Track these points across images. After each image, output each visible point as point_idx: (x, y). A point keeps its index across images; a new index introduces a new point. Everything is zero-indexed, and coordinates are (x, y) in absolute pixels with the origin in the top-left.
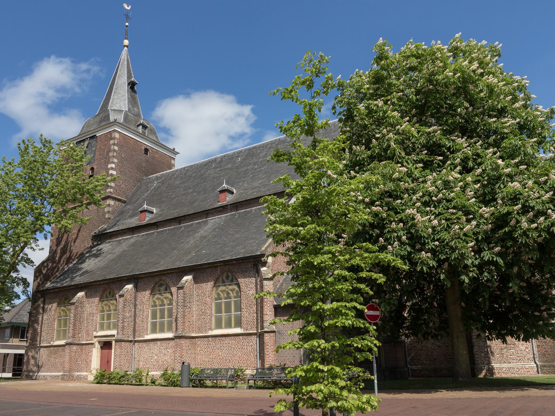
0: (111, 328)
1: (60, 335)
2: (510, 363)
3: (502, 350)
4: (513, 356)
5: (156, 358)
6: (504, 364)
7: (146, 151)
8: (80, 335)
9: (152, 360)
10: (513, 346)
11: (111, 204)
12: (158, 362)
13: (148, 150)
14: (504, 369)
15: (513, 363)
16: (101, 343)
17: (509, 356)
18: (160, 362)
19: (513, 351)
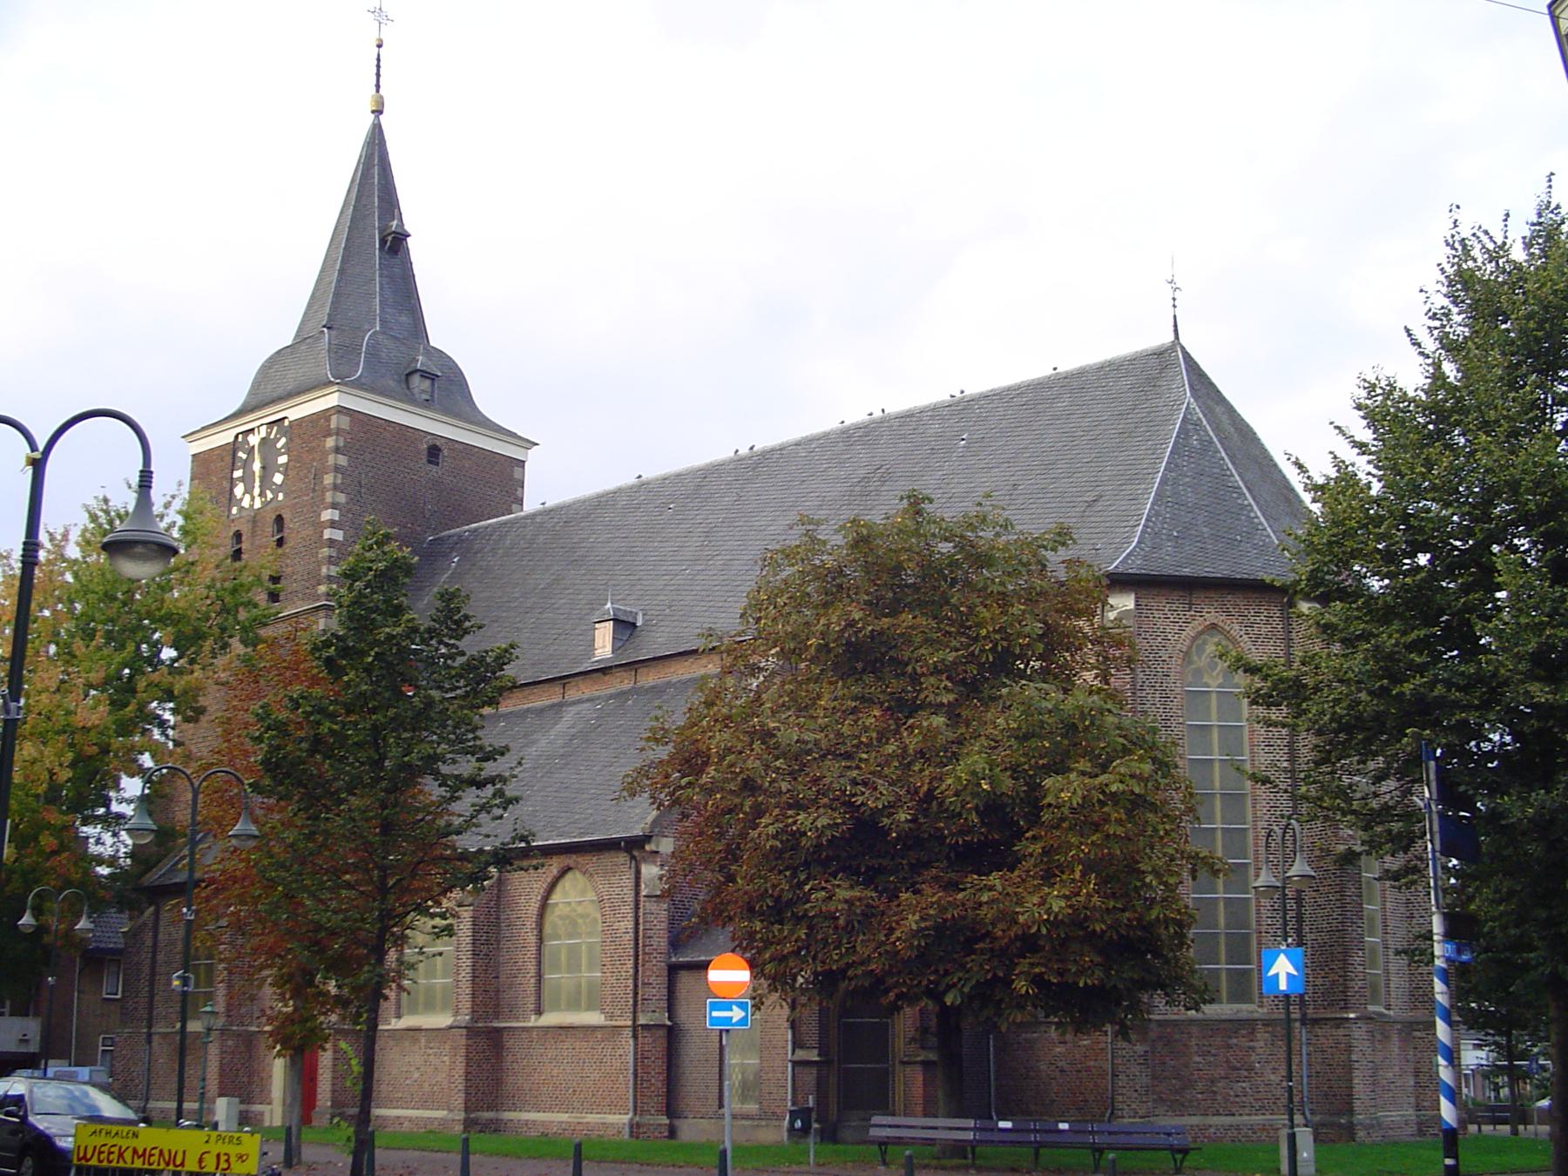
0: (92, 1170)
1: (505, 1028)
2: (1233, 1115)
3: (1212, 1082)
4: (1244, 1099)
5: (416, 1075)
6: (1215, 1118)
7: (434, 452)
8: (243, 1010)
9: (407, 1082)
10: (1246, 1073)
11: (338, 500)
12: (421, 1086)
13: (440, 450)
14: (1212, 1130)
15: (1241, 1115)
16: (268, 1101)
17: (1232, 1099)
18: (427, 1088)
19: (1244, 1085)
